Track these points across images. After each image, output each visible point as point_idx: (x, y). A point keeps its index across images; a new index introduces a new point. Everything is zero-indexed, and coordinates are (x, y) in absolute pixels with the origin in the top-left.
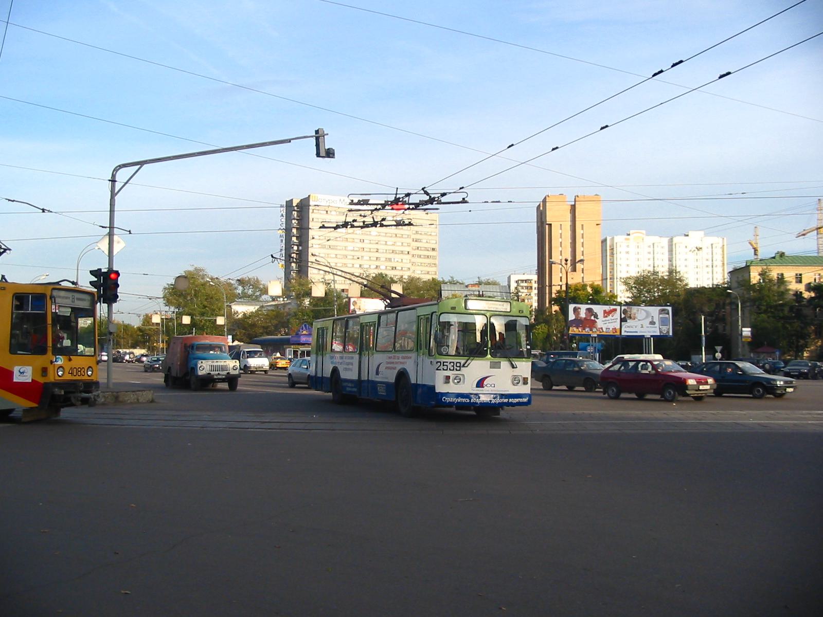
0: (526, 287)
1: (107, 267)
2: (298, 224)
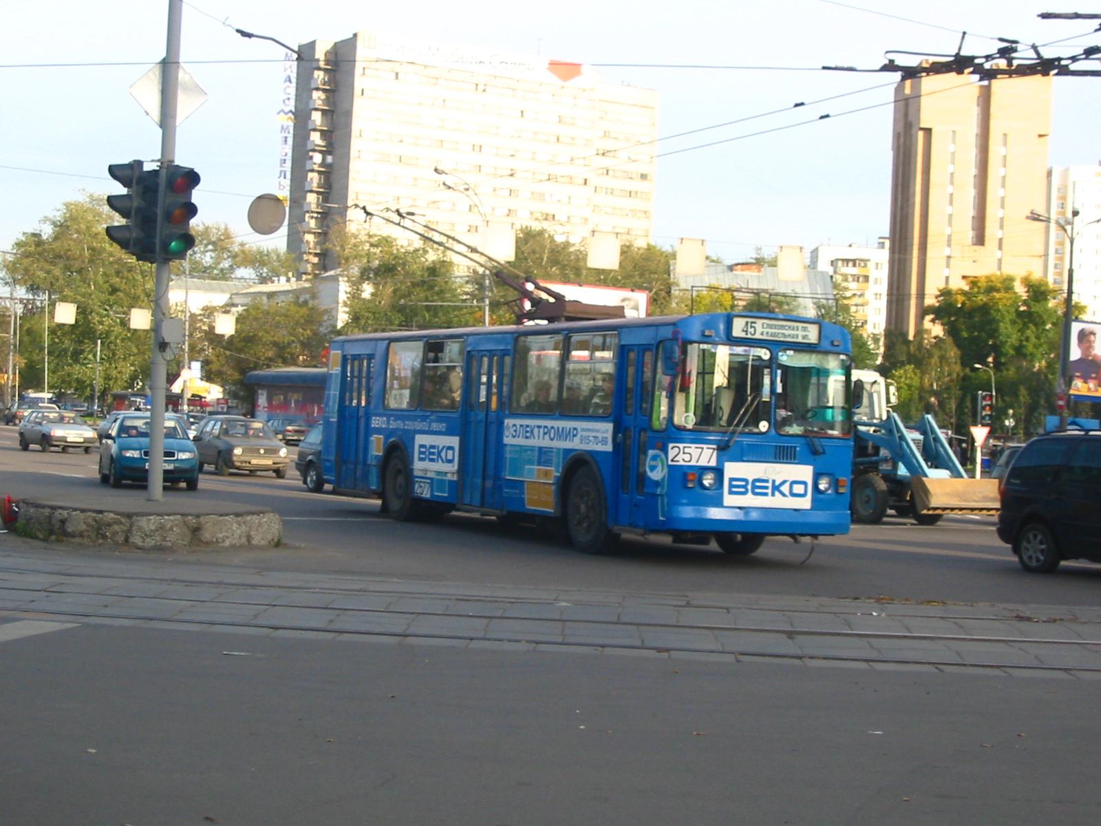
0: (853, 276)
1: (159, 157)
2: (327, 101)
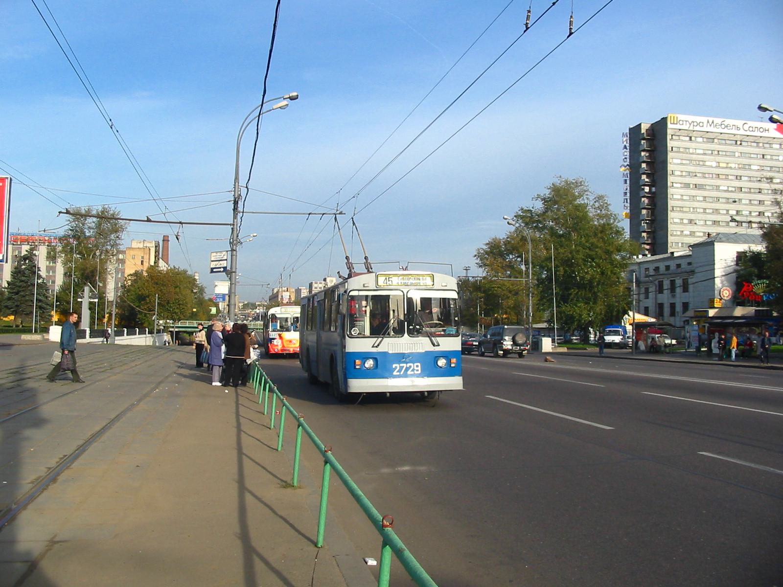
2: (650, 157)
